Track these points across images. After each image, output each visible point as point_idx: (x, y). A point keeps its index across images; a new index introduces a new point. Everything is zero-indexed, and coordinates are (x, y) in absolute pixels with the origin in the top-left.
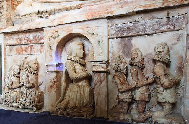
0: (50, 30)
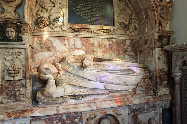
0: (88, 113)
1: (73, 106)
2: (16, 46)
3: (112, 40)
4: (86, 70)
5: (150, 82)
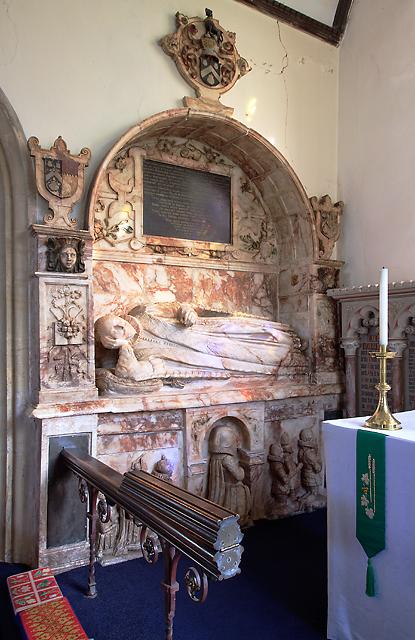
1: (170, 398)
2: (72, 281)
3: (228, 272)
4: (187, 330)
5: (302, 358)
